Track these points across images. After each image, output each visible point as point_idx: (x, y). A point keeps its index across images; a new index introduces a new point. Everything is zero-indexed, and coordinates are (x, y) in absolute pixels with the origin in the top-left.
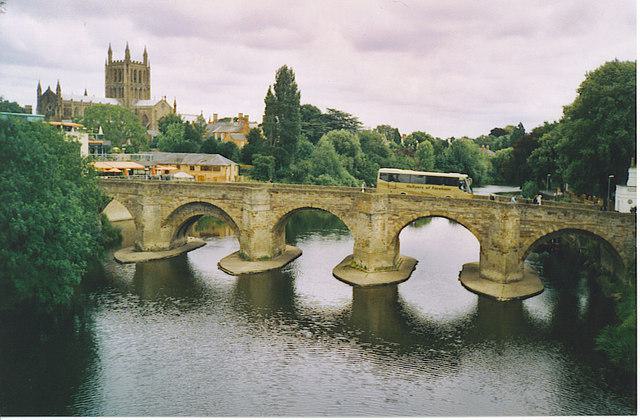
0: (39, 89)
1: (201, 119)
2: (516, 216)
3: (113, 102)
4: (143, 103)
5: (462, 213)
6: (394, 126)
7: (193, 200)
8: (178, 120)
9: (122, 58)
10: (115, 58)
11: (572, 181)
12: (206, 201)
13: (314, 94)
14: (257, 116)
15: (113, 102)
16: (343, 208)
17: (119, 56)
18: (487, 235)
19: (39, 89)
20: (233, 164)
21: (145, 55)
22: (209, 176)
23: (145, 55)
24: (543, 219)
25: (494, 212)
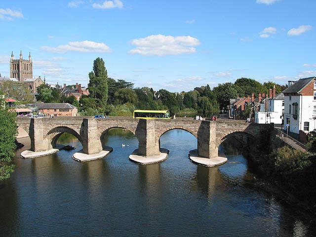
1: (58, 86)
2: (214, 127)
3: (15, 80)
6: (150, 87)
7: (59, 126)
8: (47, 86)
10: (14, 58)
11: (276, 131)
12: (66, 126)
13: (114, 73)
14: (85, 82)
15: (15, 80)
22: (64, 114)
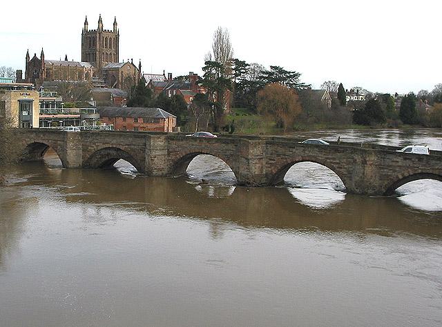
0: (28, 55)
3: (87, 65)
4: (113, 65)
5: (329, 159)
7: (107, 146)
9: (95, 28)
16: (228, 153)
17: (93, 26)
18: (350, 178)
19: (28, 55)
20: (171, 116)
21: (115, 24)
23: (115, 24)
24: (400, 164)
25: (356, 157)
